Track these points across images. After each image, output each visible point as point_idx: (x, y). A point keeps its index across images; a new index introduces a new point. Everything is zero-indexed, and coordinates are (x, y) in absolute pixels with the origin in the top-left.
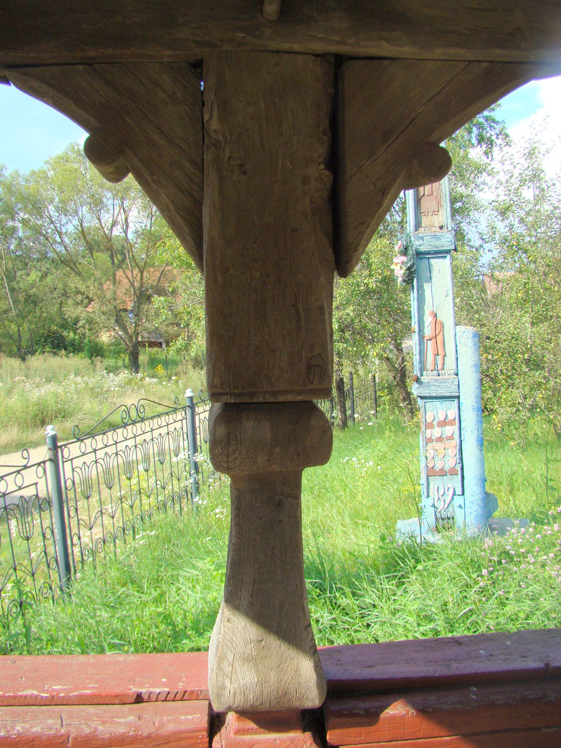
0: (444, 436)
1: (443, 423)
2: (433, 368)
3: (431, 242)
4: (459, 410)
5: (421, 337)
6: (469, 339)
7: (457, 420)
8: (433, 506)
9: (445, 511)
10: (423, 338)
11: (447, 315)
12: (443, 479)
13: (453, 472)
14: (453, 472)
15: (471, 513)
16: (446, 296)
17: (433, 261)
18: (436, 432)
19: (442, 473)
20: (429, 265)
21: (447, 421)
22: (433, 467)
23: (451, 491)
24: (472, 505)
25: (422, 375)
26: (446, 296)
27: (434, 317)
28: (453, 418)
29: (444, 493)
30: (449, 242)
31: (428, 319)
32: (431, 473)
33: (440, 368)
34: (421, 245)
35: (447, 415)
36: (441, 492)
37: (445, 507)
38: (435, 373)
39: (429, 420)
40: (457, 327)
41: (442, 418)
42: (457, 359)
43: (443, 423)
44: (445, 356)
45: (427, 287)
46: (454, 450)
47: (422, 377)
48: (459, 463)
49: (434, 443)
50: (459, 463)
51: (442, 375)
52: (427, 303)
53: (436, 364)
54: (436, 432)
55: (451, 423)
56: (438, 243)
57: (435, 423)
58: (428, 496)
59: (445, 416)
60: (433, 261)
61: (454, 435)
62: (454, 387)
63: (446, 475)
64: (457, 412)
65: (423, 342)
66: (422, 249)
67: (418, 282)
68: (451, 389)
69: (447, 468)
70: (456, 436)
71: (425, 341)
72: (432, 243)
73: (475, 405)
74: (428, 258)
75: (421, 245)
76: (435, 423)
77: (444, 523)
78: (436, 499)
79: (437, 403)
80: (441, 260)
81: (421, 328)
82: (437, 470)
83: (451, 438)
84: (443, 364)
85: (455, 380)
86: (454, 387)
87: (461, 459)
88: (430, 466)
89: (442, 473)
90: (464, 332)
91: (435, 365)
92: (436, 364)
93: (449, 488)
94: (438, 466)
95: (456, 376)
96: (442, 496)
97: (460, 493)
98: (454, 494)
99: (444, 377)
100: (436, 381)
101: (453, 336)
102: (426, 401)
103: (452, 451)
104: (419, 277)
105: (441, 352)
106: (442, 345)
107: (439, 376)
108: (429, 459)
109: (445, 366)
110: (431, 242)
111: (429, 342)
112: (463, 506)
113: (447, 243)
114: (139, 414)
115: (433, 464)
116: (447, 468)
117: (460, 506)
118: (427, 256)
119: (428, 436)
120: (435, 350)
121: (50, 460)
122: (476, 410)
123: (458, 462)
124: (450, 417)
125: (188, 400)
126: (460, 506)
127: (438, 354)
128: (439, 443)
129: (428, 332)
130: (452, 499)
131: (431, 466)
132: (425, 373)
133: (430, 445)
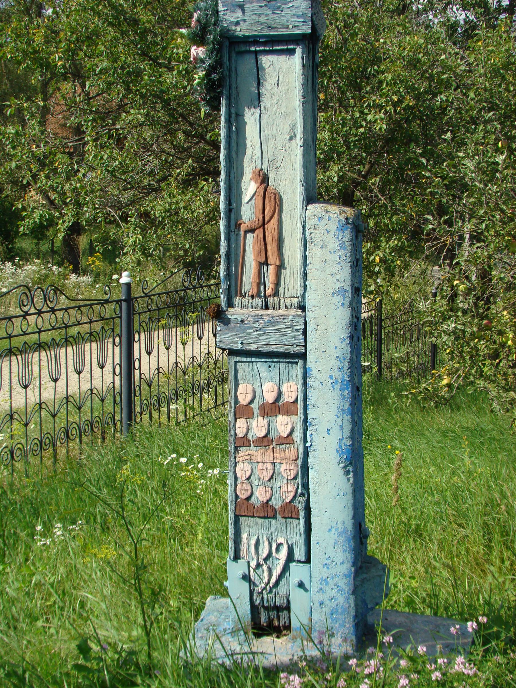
0: (273, 435)
1: (275, 408)
2: (255, 292)
3: (260, 15)
4: (305, 383)
5: (233, 223)
6: (331, 234)
7: (300, 404)
8: (246, 578)
9: (270, 592)
10: (238, 226)
11: (290, 183)
12: (269, 525)
13: (288, 512)
14: (288, 512)
15: (321, 603)
16: (291, 139)
17: (266, 60)
18: (258, 426)
19: (267, 512)
20: (258, 68)
21: (280, 403)
22: (248, 499)
23: (284, 553)
24: (324, 586)
25: (230, 305)
26: (291, 139)
27: (262, 182)
28: (292, 400)
29: (269, 555)
30: (298, 17)
31: (250, 188)
32: (245, 509)
33: (269, 291)
34: (237, 23)
35: (280, 393)
36: (264, 552)
37: (271, 584)
38: (259, 301)
39: (243, 399)
40: (310, 207)
41: (270, 398)
42: (305, 275)
43: (275, 408)
44: (281, 267)
45: (250, 117)
46: (293, 467)
47: (231, 310)
48: (302, 495)
49: (252, 450)
50: (302, 495)
51: (274, 308)
52: (249, 151)
53: (260, 282)
54: (258, 426)
55: (288, 410)
56: (275, 19)
57: (255, 407)
58: (237, 557)
59: (275, 394)
60: (266, 60)
61: (294, 436)
62: (295, 334)
63: (274, 517)
64: (300, 386)
65: (238, 235)
66: (240, 31)
67: (229, 105)
68: (289, 338)
69: (276, 503)
70: (297, 436)
71: (242, 233)
72: (262, 19)
73: (338, 375)
74: (256, 53)
75: (237, 23)
76: (255, 407)
77: (268, 619)
78: (253, 564)
79: (260, 366)
80: (283, 58)
81: (234, 205)
82: (257, 505)
83: (287, 440)
84: (277, 284)
85: (298, 319)
86: (294, 334)
87: (306, 486)
88: (243, 496)
89: (267, 512)
90: (321, 218)
91: (259, 285)
92: (260, 282)
93: (279, 545)
94: (260, 496)
95: (300, 312)
96: (266, 559)
97: (303, 559)
98: (290, 558)
99: (277, 312)
100: (258, 319)
101: (299, 226)
102: (237, 359)
103: (287, 469)
104: (233, 96)
105: (273, 258)
106: (275, 244)
107: (267, 308)
108: (239, 481)
109: (281, 290)
110: (260, 15)
111: (249, 236)
112: (307, 586)
113: (295, 19)
114: (49, 303)
115: (249, 492)
116: (276, 503)
117: (301, 585)
118: (253, 49)
119: (241, 432)
120: (259, 253)
121: (125, 300)
122: (338, 386)
123: (300, 491)
124: (288, 396)
125: (124, 289)
126: (301, 585)
127: (266, 263)
128: (261, 450)
129: (248, 213)
130: (286, 569)
131: (244, 497)
132: (237, 301)
133: (244, 451)
